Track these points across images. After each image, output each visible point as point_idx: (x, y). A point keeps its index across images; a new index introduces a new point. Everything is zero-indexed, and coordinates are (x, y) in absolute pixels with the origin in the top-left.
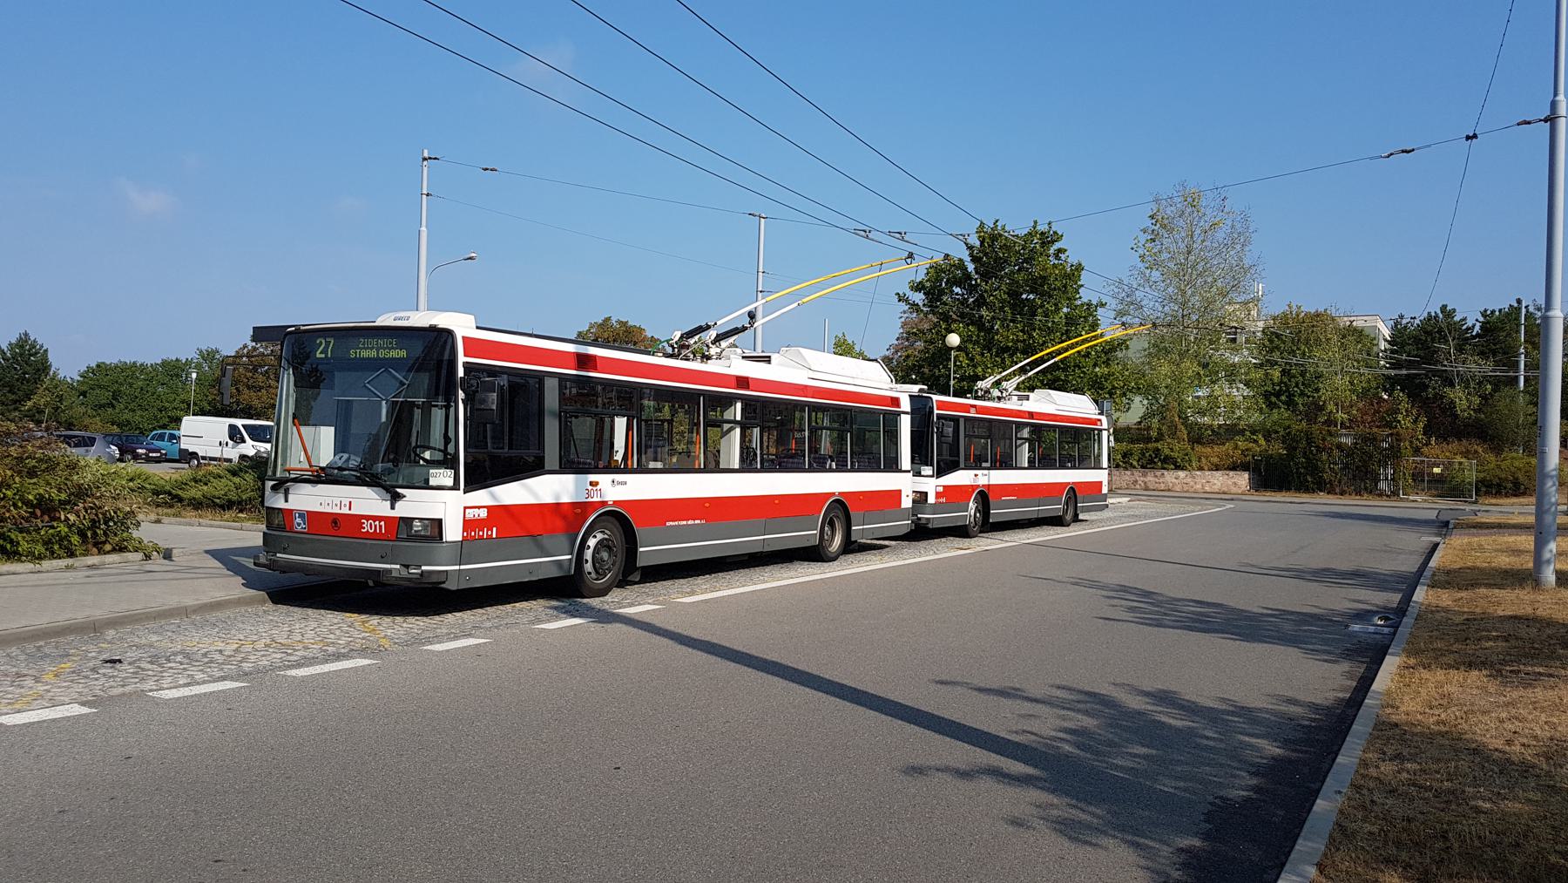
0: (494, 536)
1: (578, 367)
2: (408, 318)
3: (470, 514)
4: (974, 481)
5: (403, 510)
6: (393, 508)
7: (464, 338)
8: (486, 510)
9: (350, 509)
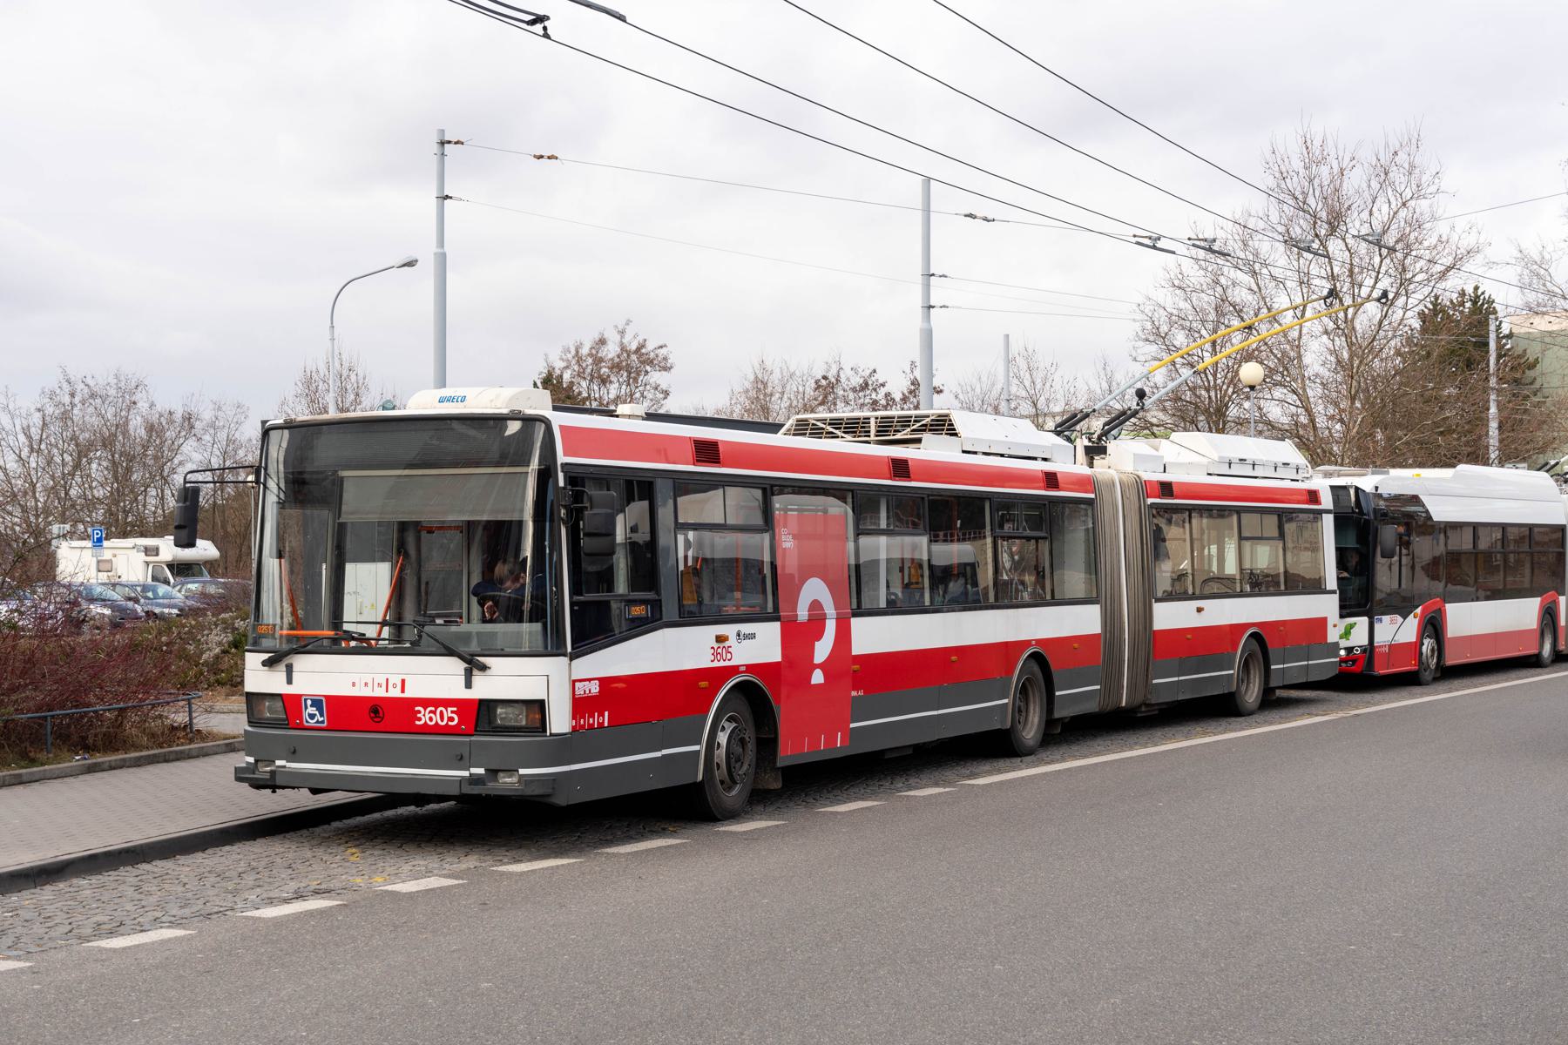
0: (606, 724)
1: (698, 461)
2: (463, 399)
3: (581, 689)
4: (716, 655)
5: (485, 688)
6: (468, 685)
7: (561, 427)
8: (597, 682)
9: (403, 691)
